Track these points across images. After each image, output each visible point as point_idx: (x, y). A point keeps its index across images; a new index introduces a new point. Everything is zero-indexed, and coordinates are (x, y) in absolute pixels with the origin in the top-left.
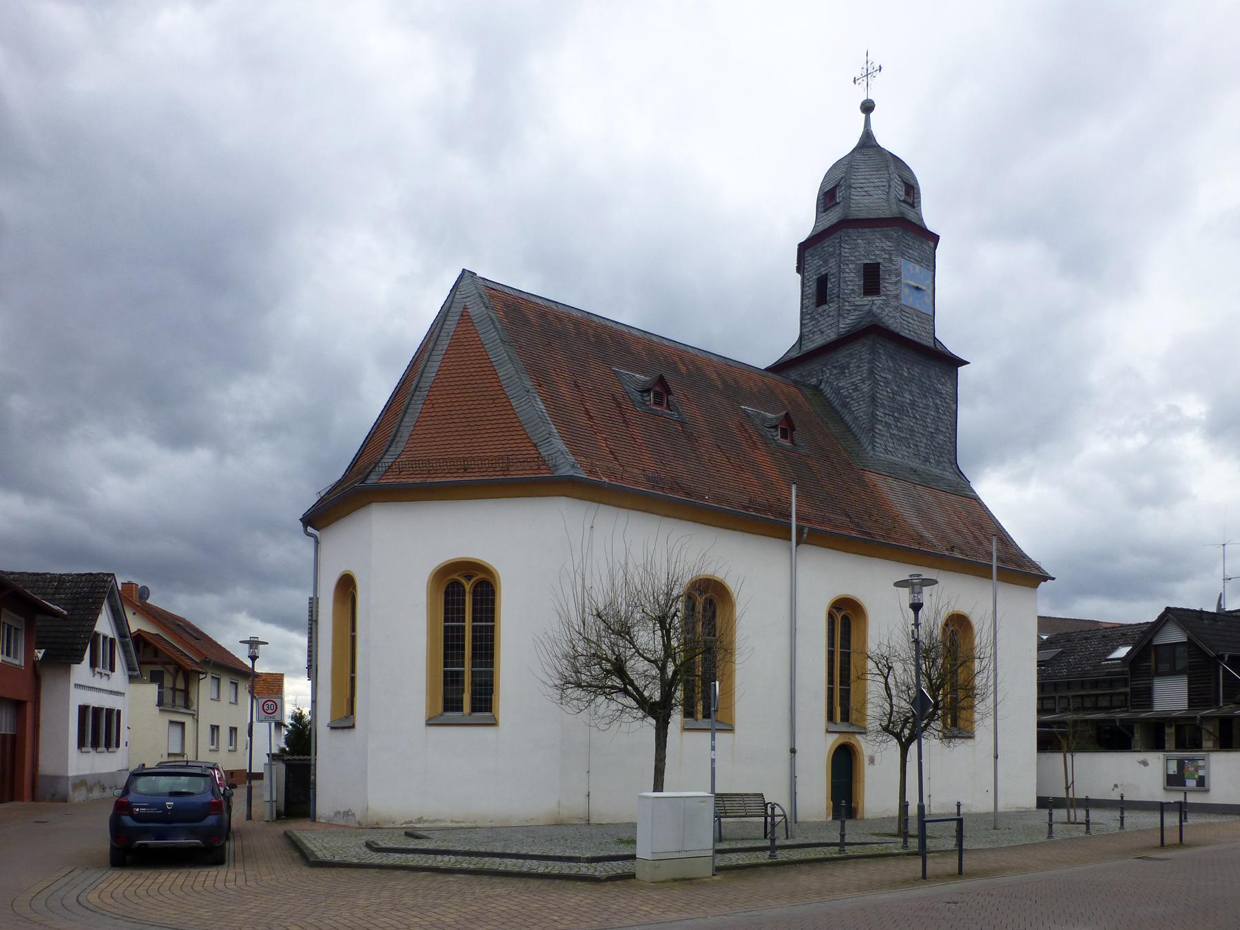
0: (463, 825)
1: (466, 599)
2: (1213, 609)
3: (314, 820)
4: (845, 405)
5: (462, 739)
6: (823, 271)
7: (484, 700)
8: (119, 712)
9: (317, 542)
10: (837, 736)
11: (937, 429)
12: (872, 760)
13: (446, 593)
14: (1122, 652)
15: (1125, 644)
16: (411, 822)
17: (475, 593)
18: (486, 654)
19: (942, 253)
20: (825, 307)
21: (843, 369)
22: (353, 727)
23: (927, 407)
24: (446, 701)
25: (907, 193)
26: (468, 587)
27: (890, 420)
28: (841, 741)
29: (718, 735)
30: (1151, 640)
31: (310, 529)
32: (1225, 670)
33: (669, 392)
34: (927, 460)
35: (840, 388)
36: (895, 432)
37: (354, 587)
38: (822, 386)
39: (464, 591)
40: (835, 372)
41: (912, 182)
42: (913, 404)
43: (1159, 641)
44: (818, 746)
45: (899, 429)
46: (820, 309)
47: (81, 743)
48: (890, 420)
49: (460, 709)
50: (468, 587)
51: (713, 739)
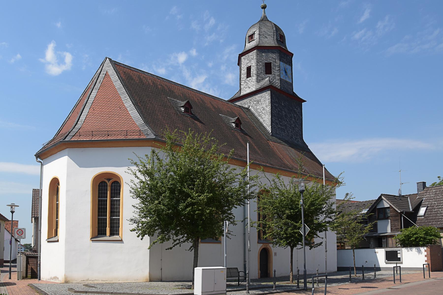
0: (107, 282)
1: (106, 190)
2: (397, 195)
3: (40, 280)
4: (260, 115)
5: (103, 247)
6: (249, 65)
7: (115, 230)
8: (58, 241)
9: (42, 165)
10: (262, 244)
11: (295, 126)
12: (275, 254)
13: (99, 186)
14: (365, 211)
15: (365, 208)
16: (84, 281)
17: (111, 186)
18: (104, 211)
19: (294, 60)
20: (250, 78)
21: (258, 102)
22: (58, 241)
23: (291, 117)
24: (99, 231)
25: (280, 38)
26: (109, 184)
27: (277, 121)
28: (263, 247)
29: (355, 250)
30: (376, 207)
31: (39, 159)
32: (404, 217)
33: (191, 108)
34: (292, 137)
35: (257, 109)
36: (279, 126)
37: (59, 184)
38: (250, 108)
39: (107, 185)
40: (255, 103)
41: (282, 34)
42: (286, 115)
43: (379, 207)
44: (255, 248)
45: (281, 125)
46: (248, 79)
47: (203, 269)
48: (277, 121)
49: (105, 234)
50: (109, 184)
51: (354, 251)
